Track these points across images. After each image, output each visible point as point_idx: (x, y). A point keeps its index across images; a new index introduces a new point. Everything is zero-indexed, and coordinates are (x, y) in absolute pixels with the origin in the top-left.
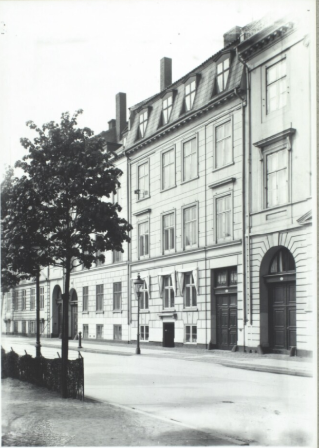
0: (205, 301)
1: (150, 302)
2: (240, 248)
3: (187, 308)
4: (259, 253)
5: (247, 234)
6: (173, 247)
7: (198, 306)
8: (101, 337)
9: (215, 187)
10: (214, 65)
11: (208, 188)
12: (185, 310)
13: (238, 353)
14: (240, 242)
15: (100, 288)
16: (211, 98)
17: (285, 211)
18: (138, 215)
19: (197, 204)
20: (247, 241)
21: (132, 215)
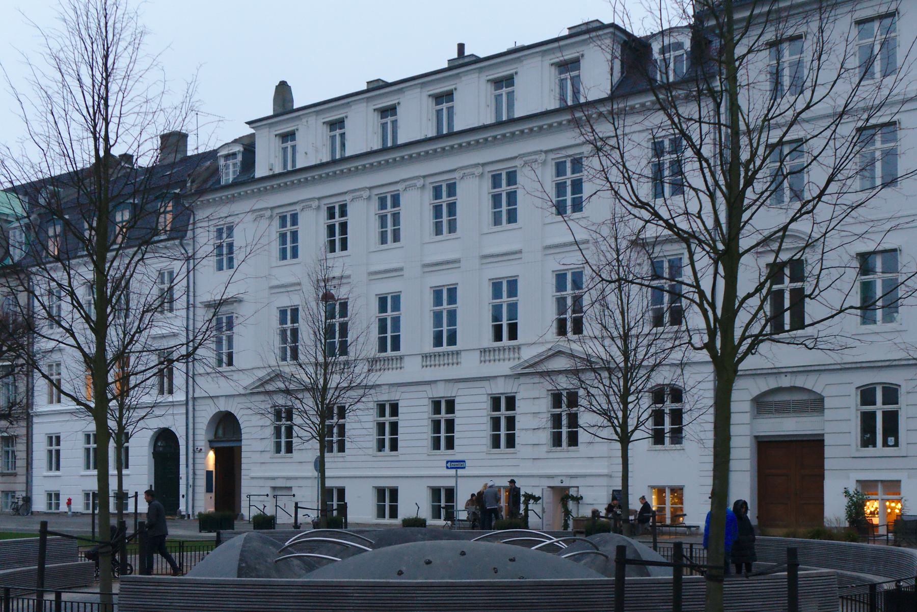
0: (459, 479)
4: (206, 413)
5: (190, 396)
20: (191, 403)
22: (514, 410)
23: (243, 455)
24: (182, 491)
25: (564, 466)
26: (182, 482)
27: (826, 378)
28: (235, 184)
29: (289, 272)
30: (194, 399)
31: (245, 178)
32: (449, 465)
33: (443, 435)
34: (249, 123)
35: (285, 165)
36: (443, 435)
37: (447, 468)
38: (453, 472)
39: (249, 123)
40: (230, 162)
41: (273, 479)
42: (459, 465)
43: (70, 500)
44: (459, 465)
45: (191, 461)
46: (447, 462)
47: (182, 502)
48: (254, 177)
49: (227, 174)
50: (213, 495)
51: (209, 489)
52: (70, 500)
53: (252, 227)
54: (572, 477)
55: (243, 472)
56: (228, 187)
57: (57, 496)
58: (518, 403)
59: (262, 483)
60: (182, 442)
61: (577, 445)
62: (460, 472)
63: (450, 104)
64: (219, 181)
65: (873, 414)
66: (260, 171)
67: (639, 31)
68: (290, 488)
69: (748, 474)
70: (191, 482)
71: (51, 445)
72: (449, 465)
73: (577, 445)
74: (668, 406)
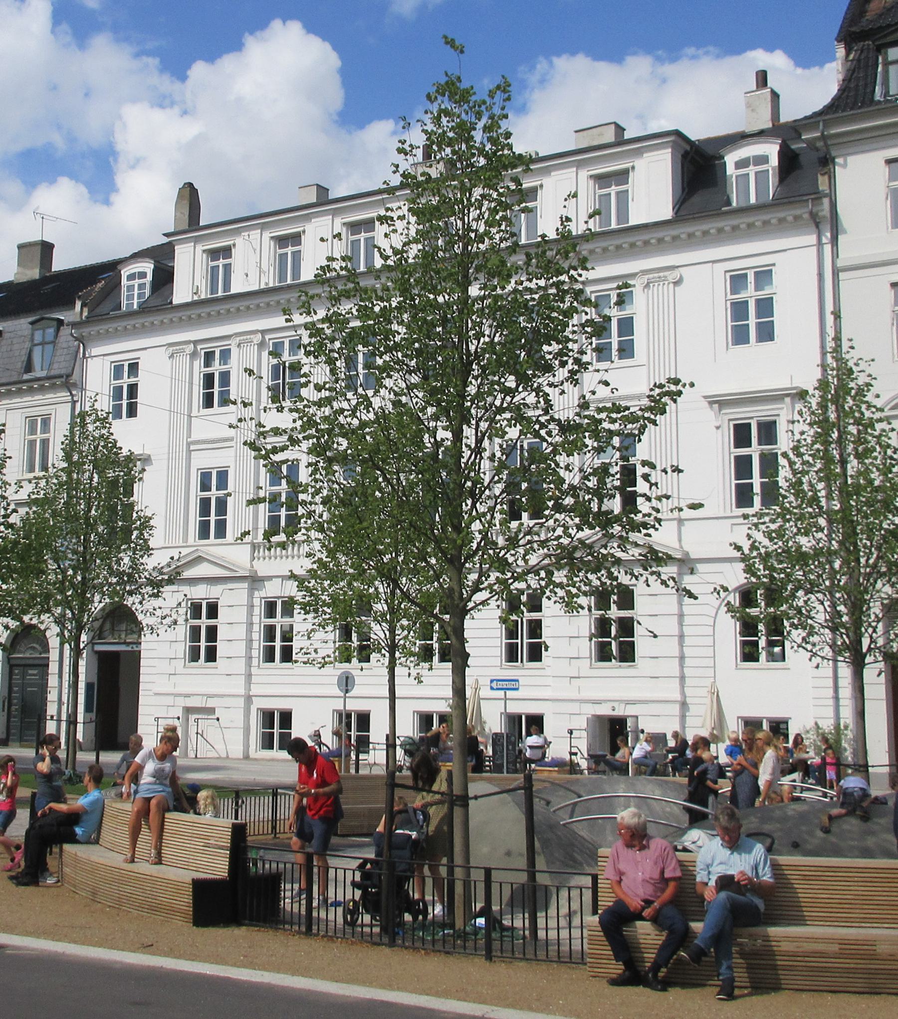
8: (14, 741)
22: (633, 609)
23: (143, 662)
25: (277, 685)
28: (145, 309)
29: (215, 423)
31: (158, 302)
32: (494, 685)
33: (203, 644)
34: (164, 235)
35: (214, 290)
36: (203, 644)
37: (492, 688)
38: (501, 694)
39: (164, 235)
40: (136, 282)
41: (187, 696)
42: (510, 685)
44: (510, 685)
46: (492, 681)
48: (171, 303)
49: (130, 297)
50: (93, 715)
53: (162, 363)
54: (628, 703)
55: (142, 686)
56: (131, 314)
58: (221, 611)
59: (170, 700)
61: (215, 661)
62: (510, 694)
63: (227, 261)
64: (119, 307)
66: (181, 293)
67: (696, 133)
68: (212, 711)
72: (494, 685)
73: (215, 661)
74: (204, 622)
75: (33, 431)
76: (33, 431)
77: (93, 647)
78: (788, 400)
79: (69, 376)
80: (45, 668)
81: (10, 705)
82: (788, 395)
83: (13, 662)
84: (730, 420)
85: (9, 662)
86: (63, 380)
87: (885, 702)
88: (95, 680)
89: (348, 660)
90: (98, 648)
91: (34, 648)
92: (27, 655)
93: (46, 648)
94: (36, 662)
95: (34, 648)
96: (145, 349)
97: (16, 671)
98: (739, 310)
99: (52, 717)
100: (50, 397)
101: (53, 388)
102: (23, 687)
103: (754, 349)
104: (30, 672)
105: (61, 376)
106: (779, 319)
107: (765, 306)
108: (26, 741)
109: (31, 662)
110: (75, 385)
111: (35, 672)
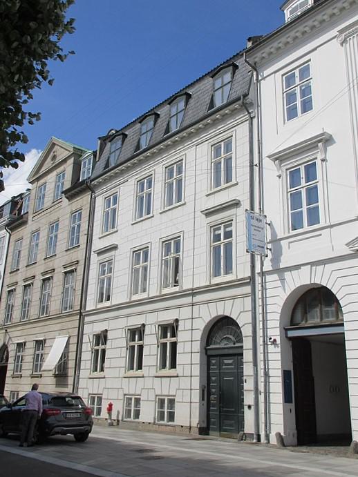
0: (190, 363)
1: (106, 365)
2: (248, 289)
3: (131, 373)
4: (278, 296)
5: (258, 270)
6: (144, 290)
7: (144, 371)
8: (214, 430)
9: (209, 213)
10: (138, 125)
11: (199, 214)
12: (157, 375)
13: (243, 445)
14: (248, 280)
15: (170, 329)
16: (309, 65)
17: (321, 235)
18: (100, 253)
19: (150, 246)
20: (258, 279)
21: (92, 253)
24: (249, 399)
26: (248, 385)
27: (197, 437)
30: (263, 274)
43: (111, 405)
45: (260, 357)
47: (249, 416)
50: (292, 406)
51: (287, 399)
52: (111, 405)
57: (100, 399)
60: (246, 331)
65: (164, 412)
69: (281, 378)
70: (261, 387)
71: (165, 337)
75: (171, 175)
76: (171, 175)
77: (286, 334)
78: (320, 144)
79: (245, 96)
80: (239, 357)
81: (209, 394)
82: (320, 141)
83: (210, 353)
84: (287, 170)
85: (206, 354)
86: (240, 102)
87: (347, 348)
88: (290, 367)
89: (99, 345)
90: (292, 334)
91: (228, 339)
92: (222, 346)
93: (239, 338)
94: (231, 352)
95: (228, 339)
96: (316, 49)
97: (214, 362)
98: (290, 97)
99: (249, 407)
100: (230, 122)
101: (234, 113)
102: (220, 376)
103: (302, 118)
104: (226, 361)
105: (239, 99)
106: (315, 95)
107: (306, 91)
108: (225, 430)
109: (226, 352)
110: (251, 104)
111: (230, 361)
